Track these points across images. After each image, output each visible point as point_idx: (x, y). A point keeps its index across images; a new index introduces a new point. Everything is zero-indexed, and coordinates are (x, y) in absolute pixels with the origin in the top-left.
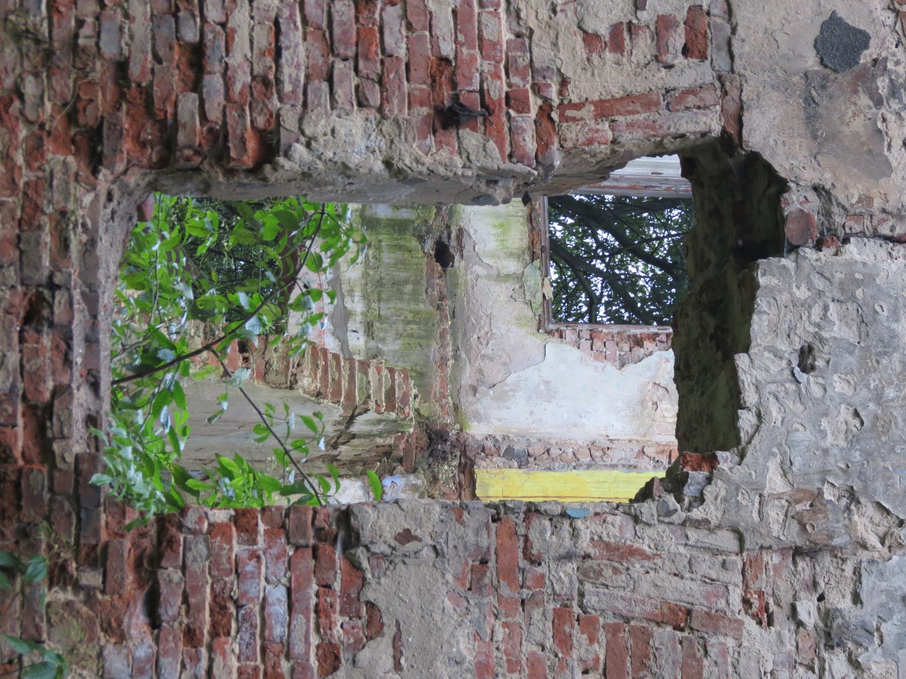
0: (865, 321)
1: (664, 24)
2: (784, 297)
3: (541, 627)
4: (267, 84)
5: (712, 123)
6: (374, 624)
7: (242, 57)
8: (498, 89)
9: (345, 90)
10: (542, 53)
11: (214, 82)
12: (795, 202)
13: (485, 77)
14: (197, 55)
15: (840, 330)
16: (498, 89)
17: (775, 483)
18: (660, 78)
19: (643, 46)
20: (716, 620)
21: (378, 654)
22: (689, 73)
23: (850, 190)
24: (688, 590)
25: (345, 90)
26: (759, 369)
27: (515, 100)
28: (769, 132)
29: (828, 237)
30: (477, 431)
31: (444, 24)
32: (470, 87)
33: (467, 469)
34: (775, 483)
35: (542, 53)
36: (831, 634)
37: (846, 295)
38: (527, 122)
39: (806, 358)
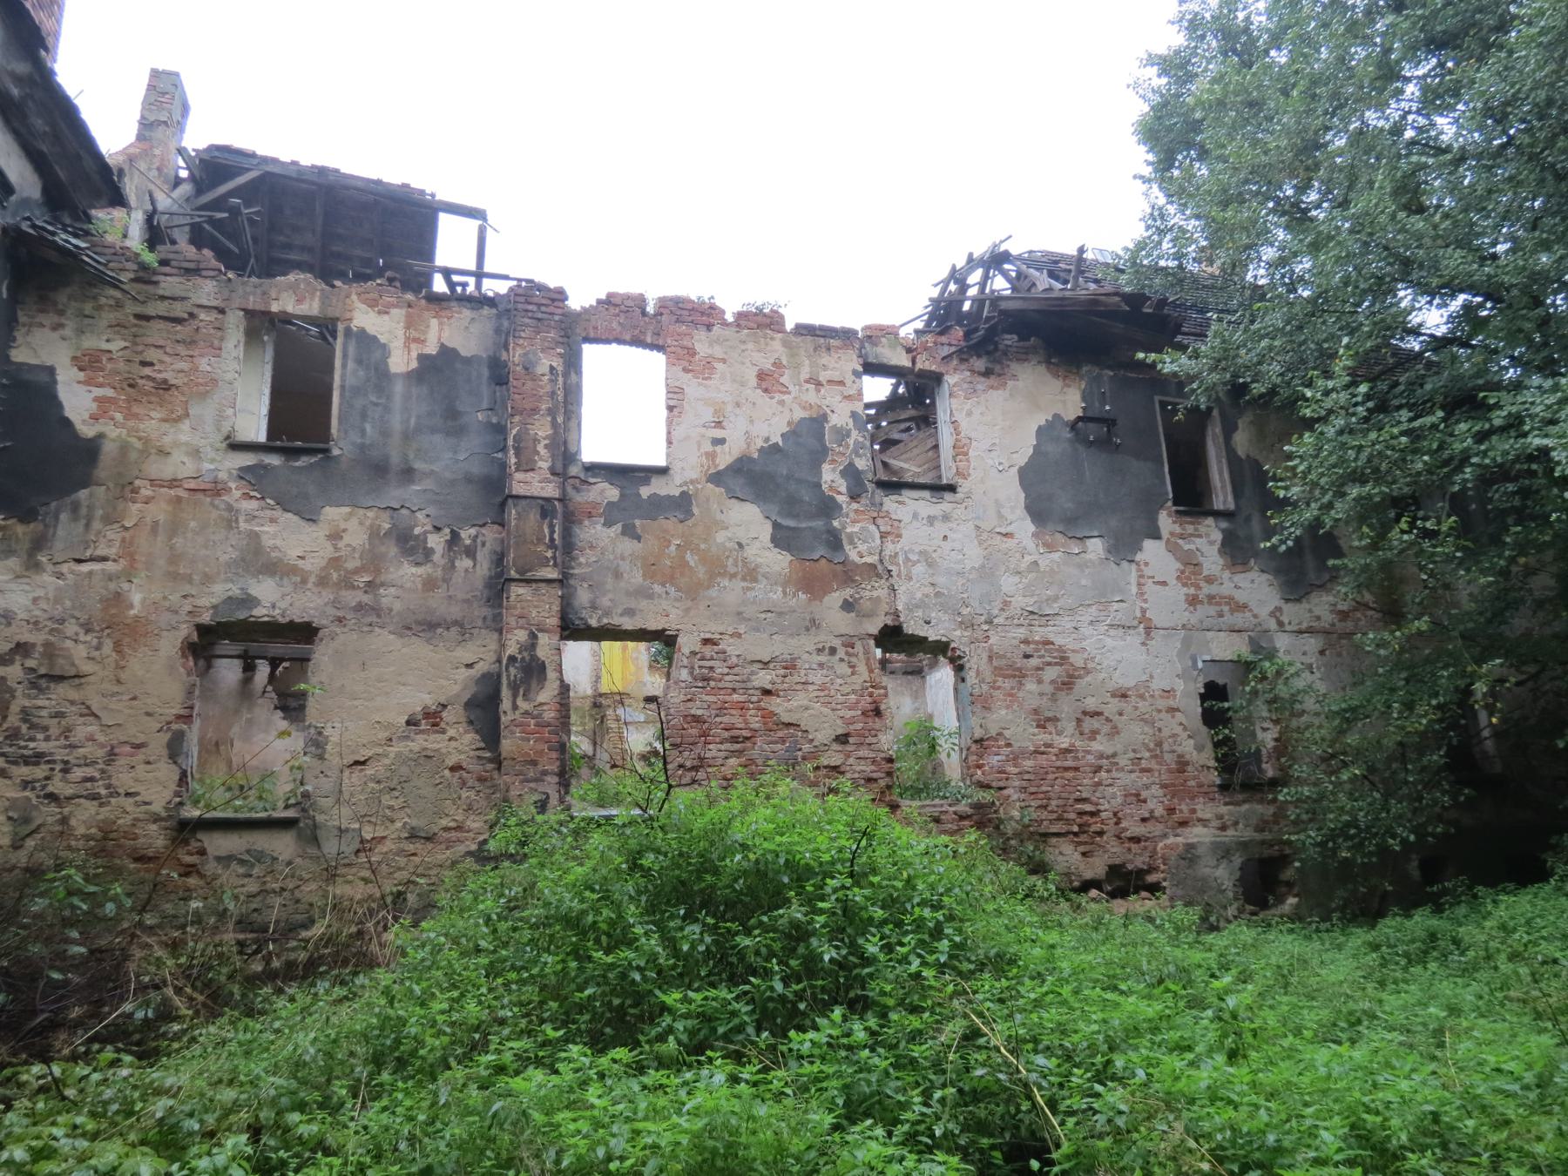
0: (917, 607)
1: (847, 653)
2: (912, 627)
3: (997, 693)
4: (874, 762)
5: (872, 642)
6: (999, 734)
7: (868, 768)
8: (869, 699)
9: (874, 740)
10: (857, 687)
11: (875, 775)
12: (890, 623)
13: (866, 702)
14: (869, 780)
15: (919, 613)
16: (869, 699)
17: (958, 633)
18: (861, 655)
19: (853, 660)
20: (991, 650)
21: (1007, 733)
22: (859, 648)
23: (885, 607)
24: (985, 656)
25: (874, 740)
26: (933, 636)
27: (871, 695)
28: (874, 629)
29: (896, 614)
30: (589, 692)
31: (852, 713)
32: (870, 707)
33: (601, 695)
34: (958, 633)
35: (857, 687)
36: (990, 622)
37: (911, 610)
38: (876, 692)
39: (928, 623)
